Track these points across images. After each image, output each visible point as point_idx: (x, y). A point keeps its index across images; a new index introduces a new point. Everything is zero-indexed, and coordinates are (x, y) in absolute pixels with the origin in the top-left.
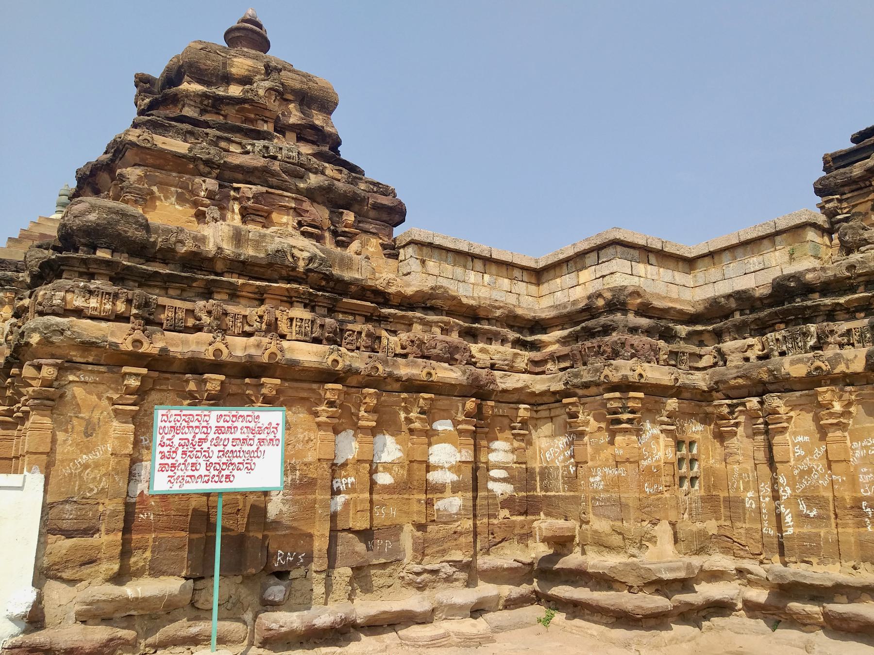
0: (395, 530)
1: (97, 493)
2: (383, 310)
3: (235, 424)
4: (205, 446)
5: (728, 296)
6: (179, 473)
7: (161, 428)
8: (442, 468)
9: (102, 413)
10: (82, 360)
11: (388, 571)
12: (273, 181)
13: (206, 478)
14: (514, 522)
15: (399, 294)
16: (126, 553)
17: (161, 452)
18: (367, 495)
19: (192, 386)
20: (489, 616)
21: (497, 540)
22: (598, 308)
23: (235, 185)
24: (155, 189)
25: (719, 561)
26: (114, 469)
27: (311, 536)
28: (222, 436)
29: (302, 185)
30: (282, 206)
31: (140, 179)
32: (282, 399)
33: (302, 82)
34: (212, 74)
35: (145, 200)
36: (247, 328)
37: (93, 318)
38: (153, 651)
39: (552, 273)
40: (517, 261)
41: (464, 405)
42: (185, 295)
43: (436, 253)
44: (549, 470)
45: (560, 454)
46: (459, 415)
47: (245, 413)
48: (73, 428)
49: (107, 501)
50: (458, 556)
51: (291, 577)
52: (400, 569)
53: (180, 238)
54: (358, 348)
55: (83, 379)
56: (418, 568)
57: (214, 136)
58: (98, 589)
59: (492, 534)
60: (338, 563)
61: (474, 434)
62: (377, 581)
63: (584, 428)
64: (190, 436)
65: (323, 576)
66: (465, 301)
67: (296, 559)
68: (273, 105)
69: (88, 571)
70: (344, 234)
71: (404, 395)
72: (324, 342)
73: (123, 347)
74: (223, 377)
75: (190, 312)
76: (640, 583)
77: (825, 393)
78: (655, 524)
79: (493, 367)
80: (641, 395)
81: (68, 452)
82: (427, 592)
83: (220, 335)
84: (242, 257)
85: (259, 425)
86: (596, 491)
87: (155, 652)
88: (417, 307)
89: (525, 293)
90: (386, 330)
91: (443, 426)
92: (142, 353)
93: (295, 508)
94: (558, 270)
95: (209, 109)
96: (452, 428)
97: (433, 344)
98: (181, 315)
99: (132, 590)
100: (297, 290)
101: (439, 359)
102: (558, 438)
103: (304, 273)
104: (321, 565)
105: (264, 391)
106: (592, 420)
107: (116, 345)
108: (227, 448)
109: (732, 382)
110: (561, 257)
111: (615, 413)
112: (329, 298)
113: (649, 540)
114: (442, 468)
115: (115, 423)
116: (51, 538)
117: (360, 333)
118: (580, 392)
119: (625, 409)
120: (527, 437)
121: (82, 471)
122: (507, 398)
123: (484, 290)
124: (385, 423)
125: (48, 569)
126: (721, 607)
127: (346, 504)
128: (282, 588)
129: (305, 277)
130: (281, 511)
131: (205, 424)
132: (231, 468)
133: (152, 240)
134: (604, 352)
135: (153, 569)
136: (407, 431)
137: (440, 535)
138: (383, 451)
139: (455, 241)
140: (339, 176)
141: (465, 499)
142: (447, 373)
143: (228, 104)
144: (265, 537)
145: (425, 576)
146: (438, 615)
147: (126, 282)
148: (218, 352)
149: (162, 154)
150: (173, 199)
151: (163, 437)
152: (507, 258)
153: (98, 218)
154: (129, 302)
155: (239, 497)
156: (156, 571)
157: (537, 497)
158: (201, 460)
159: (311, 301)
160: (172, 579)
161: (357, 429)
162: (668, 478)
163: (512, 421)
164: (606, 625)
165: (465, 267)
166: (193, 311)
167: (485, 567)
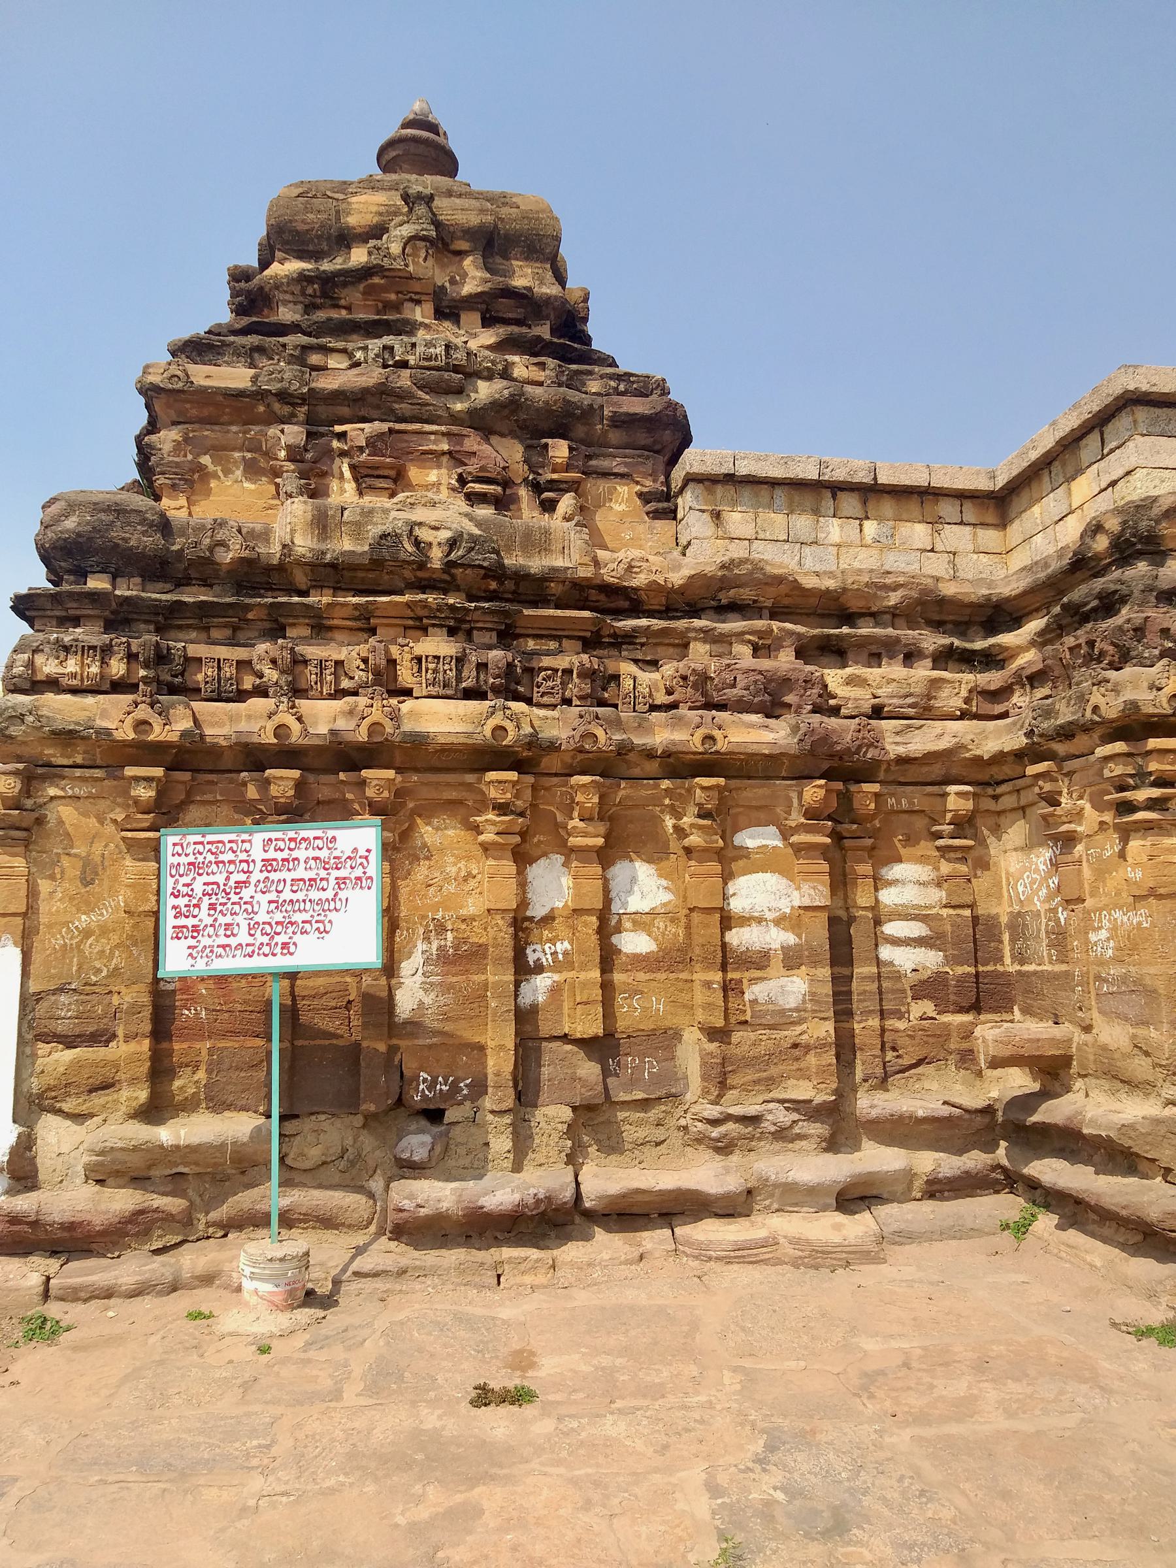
0: (664, 1039)
1: (107, 977)
2: (620, 624)
3: (295, 854)
4: (246, 893)
6: (206, 941)
7: (172, 866)
8: (760, 920)
9: (106, 846)
10: (65, 762)
11: (654, 1113)
12: (402, 407)
13: (250, 949)
14: (947, 1025)
15: (654, 587)
16: (160, 1070)
17: (174, 907)
18: (596, 974)
20: (883, 1211)
21: (906, 1061)
22: (1097, 557)
23: (338, 428)
24: (206, 460)
26: (129, 937)
27: (481, 1048)
28: (274, 876)
29: (459, 406)
30: (424, 453)
31: (177, 447)
32: (411, 805)
33: (482, 211)
34: (319, 237)
35: (190, 483)
36: (345, 684)
37: (74, 691)
38: (221, 1233)
39: (1025, 496)
40: (941, 481)
41: (800, 795)
42: (241, 636)
43: (747, 492)
44: (1024, 919)
45: (1041, 885)
46: (794, 815)
48: (62, 872)
49: (123, 990)
50: (802, 1090)
51: (446, 1120)
52: (679, 1112)
53: (218, 537)
54: (567, 702)
55: (70, 793)
56: (713, 1112)
57: (296, 347)
58: (121, 1132)
59: (894, 1049)
61: (824, 852)
62: (631, 1133)
63: (1072, 827)
65: (507, 1119)
66: (809, 582)
67: (455, 1089)
68: (424, 266)
69: (102, 1100)
70: (552, 485)
71: (665, 784)
72: (490, 695)
73: (119, 735)
74: (296, 774)
79: (877, 712)
81: (58, 911)
82: (735, 1158)
83: (285, 699)
84: (328, 556)
85: (336, 853)
86: (1102, 963)
87: (225, 1236)
88: (703, 609)
89: (971, 547)
90: (636, 661)
91: (757, 839)
92: (152, 741)
93: (448, 998)
94: (1034, 485)
95: (319, 301)
96: (780, 844)
97: (729, 678)
99: (165, 1134)
100: (424, 604)
101: (743, 707)
102: (1035, 851)
103: (444, 571)
104: (501, 1101)
105: (370, 792)
106: (1088, 806)
107: (107, 732)
108: (283, 896)
110: (1034, 455)
111: (1122, 788)
112: (491, 612)
114: (760, 920)
115: (128, 862)
116: (43, 1048)
117: (568, 672)
118: (1060, 748)
119: (1142, 777)
120: (974, 854)
121: (81, 941)
122: (913, 773)
123: (863, 554)
125: (40, 1096)
128: (427, 1139)
129: (446, 577)
130: (421, 1003)
131: (243, 856)
132: (290, 930)
133: (175, 548)
134: (1102, 653)
135: (211, 1100)
136: (681, 852)
137: (761, 1049)
138: (630, 892)
140: (540, 375)
141: (813, 980)
142: (749, 733)
143: (345, 285)
144: (393, 1050)
145: (730, 1126)
146: (761, 1202)
147: (135, 626)
149: (206, 396)
150: (239, 473)
151: (176, 882)
152: (919, 478)
153: (79, 524)
154: (131, 657)
155: (348, 979)
156: (218, 1104)
157: (1006, 974)
158: (240, 919)
159: (462, 621)
160: (243, 1116)
161: (570, 853)
163: (935, 822)
164: (1123, 1247)
165: (817, 512)
166: (250, 662)
167: (874, 1113)
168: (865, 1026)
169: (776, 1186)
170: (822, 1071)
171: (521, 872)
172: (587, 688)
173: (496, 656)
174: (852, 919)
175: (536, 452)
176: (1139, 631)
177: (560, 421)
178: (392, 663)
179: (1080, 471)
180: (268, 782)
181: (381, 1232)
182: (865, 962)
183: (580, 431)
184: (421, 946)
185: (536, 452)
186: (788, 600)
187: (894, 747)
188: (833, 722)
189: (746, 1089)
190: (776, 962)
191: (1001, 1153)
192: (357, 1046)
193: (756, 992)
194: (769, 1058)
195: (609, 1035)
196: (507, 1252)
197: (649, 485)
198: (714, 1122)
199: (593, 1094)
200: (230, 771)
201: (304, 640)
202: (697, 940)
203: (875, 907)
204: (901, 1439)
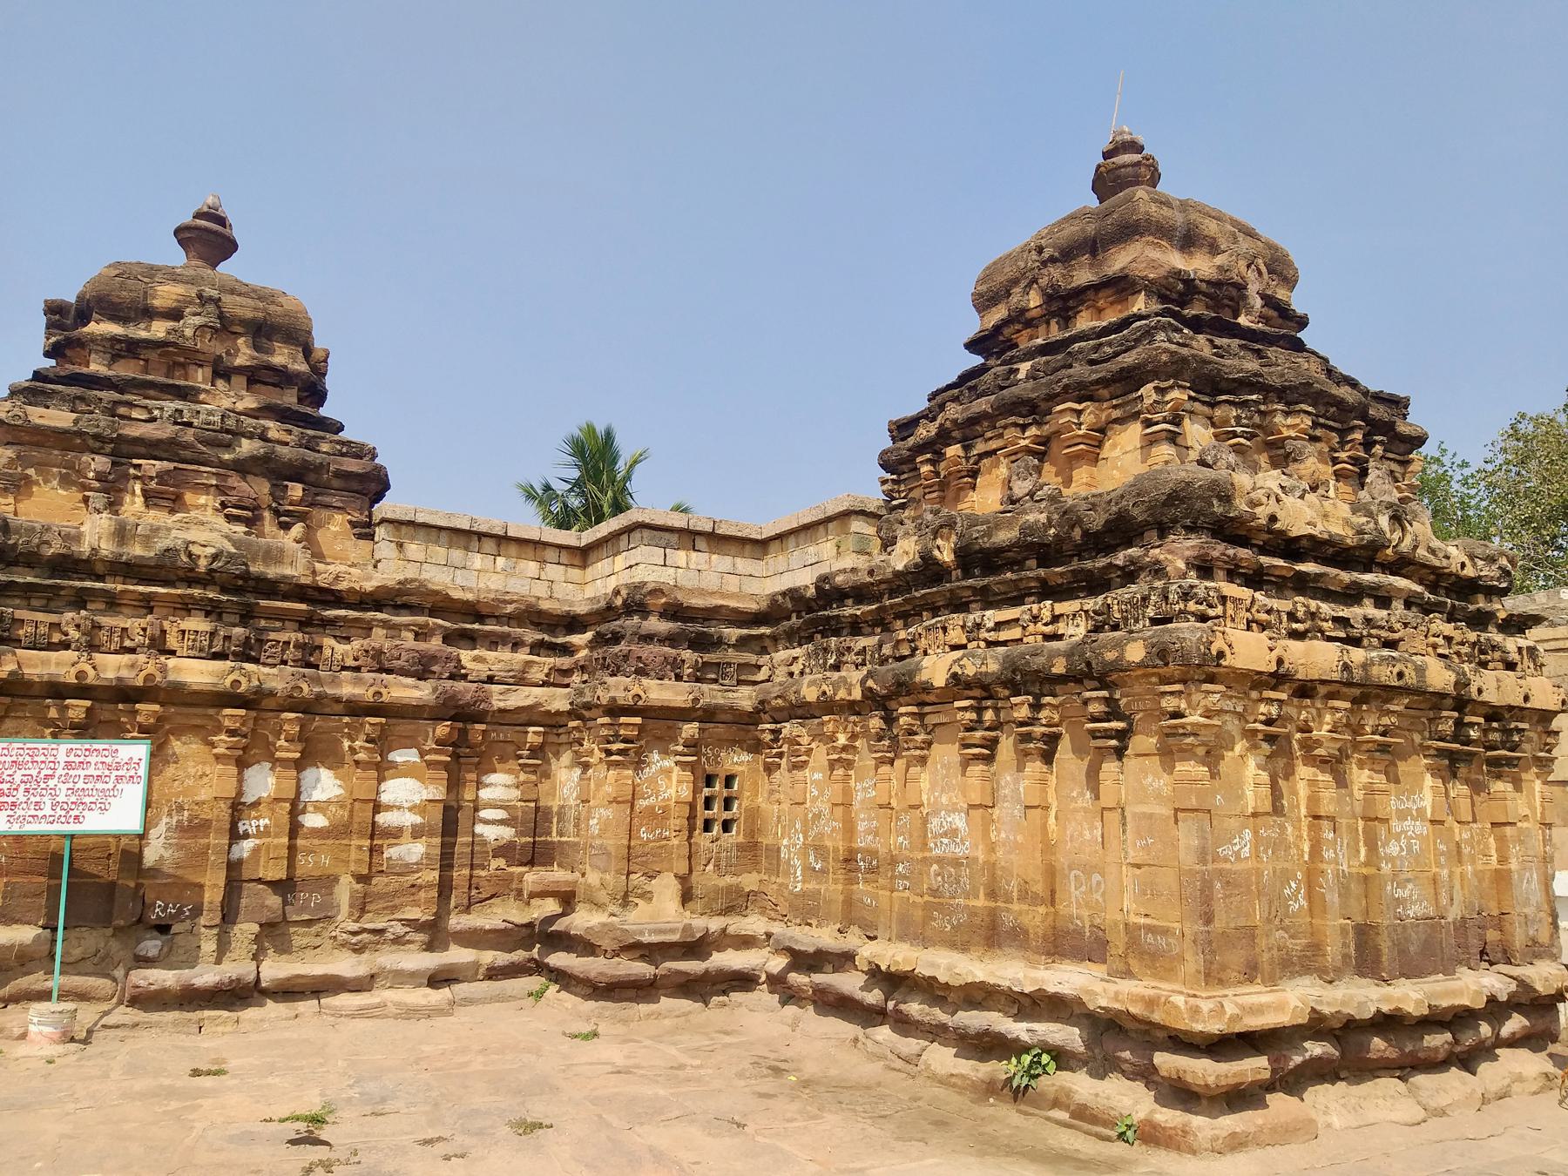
0: (327, 882)
4: (51, 783)
5: (784, 594)
6: (20, 812)
8: (399, 808)
11: (314, 929)
15: (351, 591)
18: (285, 840)
19: (53, 713)
20: (457, 987)
21: (484, 896)
23: (135, 461)
24: (31, 471)
25: (754, 924)
27: (201, 886)
29: (227, 457)
36: (127, 643)
42: (53, 604)
43: (422, 532)
47: (101, 747)
52: (332, 927)
54: (284, 662)
60: (241, 917)
61: (446, 766)
62: (297, 941)
64: (34, 772)
65: (215, 931)
66: (456, 594)
67: (180, 911)
70: (288, 513)
71: (346, 719)
74: (88, 703)
75: (55, 626)
76: (616, 947)
77: (829, 723)
78: (652, 877)
79: (491, 680)
80: (638, 720)
82: (365, 956)
93: (181, 854)
97: (396, 653)
98: (43, 630)
100: (191, 596)
105: (139, 719)
109: (774, 703)
113: (641, 896)
114: (399, 808)
117: (287, 643)
118: (587, 714)
119: (617, 737)
122: (508, 718)
123: (495, 577)
124: (312, 753)
126: (743, 981)
127: (256, 851)
128: (159, 943)
130: (162, 857)
137: (391, 888)
138: (315, 788)
139: (450, 516)
140: (288, 438)
144: (139, 886)
145: (365, 935)
146: (379, 982)
148: (81, 675)
157: (552, 843)
158: (45, 799)
161: (276, 762)
162: (678, 822)
165: (467, 549)
168: (460, 874)
169: (390, 972)
170: (427, 901)
171: (240, 773)
172: (299, 655)
173: (238, 631)
174: (460, 808)
175: (278, 492)
176: (626, 657)
177: (298, 472)
178: (164, 632)
179: (619, 553)
180: (67, 707)
181: (120, 1002)
182: (466, 834)
183: (312, 477)
184: (165, 820)
185: (278, 492)
186: (441, 605)
187: (497, 704)
188: (460, 685)
189: (377, 912)
190: (407, 834)
191: (535, 953)
192: (113, 884)
193: (392, 852)
194: (395, 894)
195: (290, 878)
196: (207, 1013)
197: (357, 516)
198: (355, 933)
199: (275, 916)
200: (36, 697)
201: (102, 612)
202: (356, 819)
203: (476, 800)
204: (426, 1076)
